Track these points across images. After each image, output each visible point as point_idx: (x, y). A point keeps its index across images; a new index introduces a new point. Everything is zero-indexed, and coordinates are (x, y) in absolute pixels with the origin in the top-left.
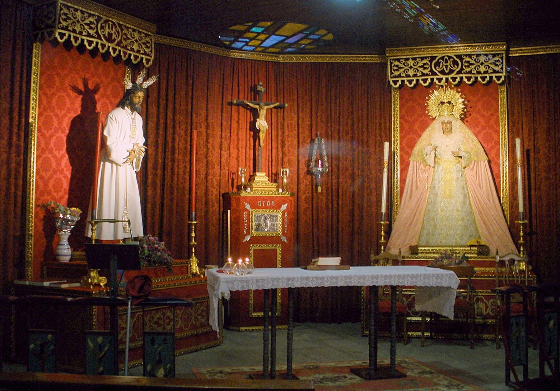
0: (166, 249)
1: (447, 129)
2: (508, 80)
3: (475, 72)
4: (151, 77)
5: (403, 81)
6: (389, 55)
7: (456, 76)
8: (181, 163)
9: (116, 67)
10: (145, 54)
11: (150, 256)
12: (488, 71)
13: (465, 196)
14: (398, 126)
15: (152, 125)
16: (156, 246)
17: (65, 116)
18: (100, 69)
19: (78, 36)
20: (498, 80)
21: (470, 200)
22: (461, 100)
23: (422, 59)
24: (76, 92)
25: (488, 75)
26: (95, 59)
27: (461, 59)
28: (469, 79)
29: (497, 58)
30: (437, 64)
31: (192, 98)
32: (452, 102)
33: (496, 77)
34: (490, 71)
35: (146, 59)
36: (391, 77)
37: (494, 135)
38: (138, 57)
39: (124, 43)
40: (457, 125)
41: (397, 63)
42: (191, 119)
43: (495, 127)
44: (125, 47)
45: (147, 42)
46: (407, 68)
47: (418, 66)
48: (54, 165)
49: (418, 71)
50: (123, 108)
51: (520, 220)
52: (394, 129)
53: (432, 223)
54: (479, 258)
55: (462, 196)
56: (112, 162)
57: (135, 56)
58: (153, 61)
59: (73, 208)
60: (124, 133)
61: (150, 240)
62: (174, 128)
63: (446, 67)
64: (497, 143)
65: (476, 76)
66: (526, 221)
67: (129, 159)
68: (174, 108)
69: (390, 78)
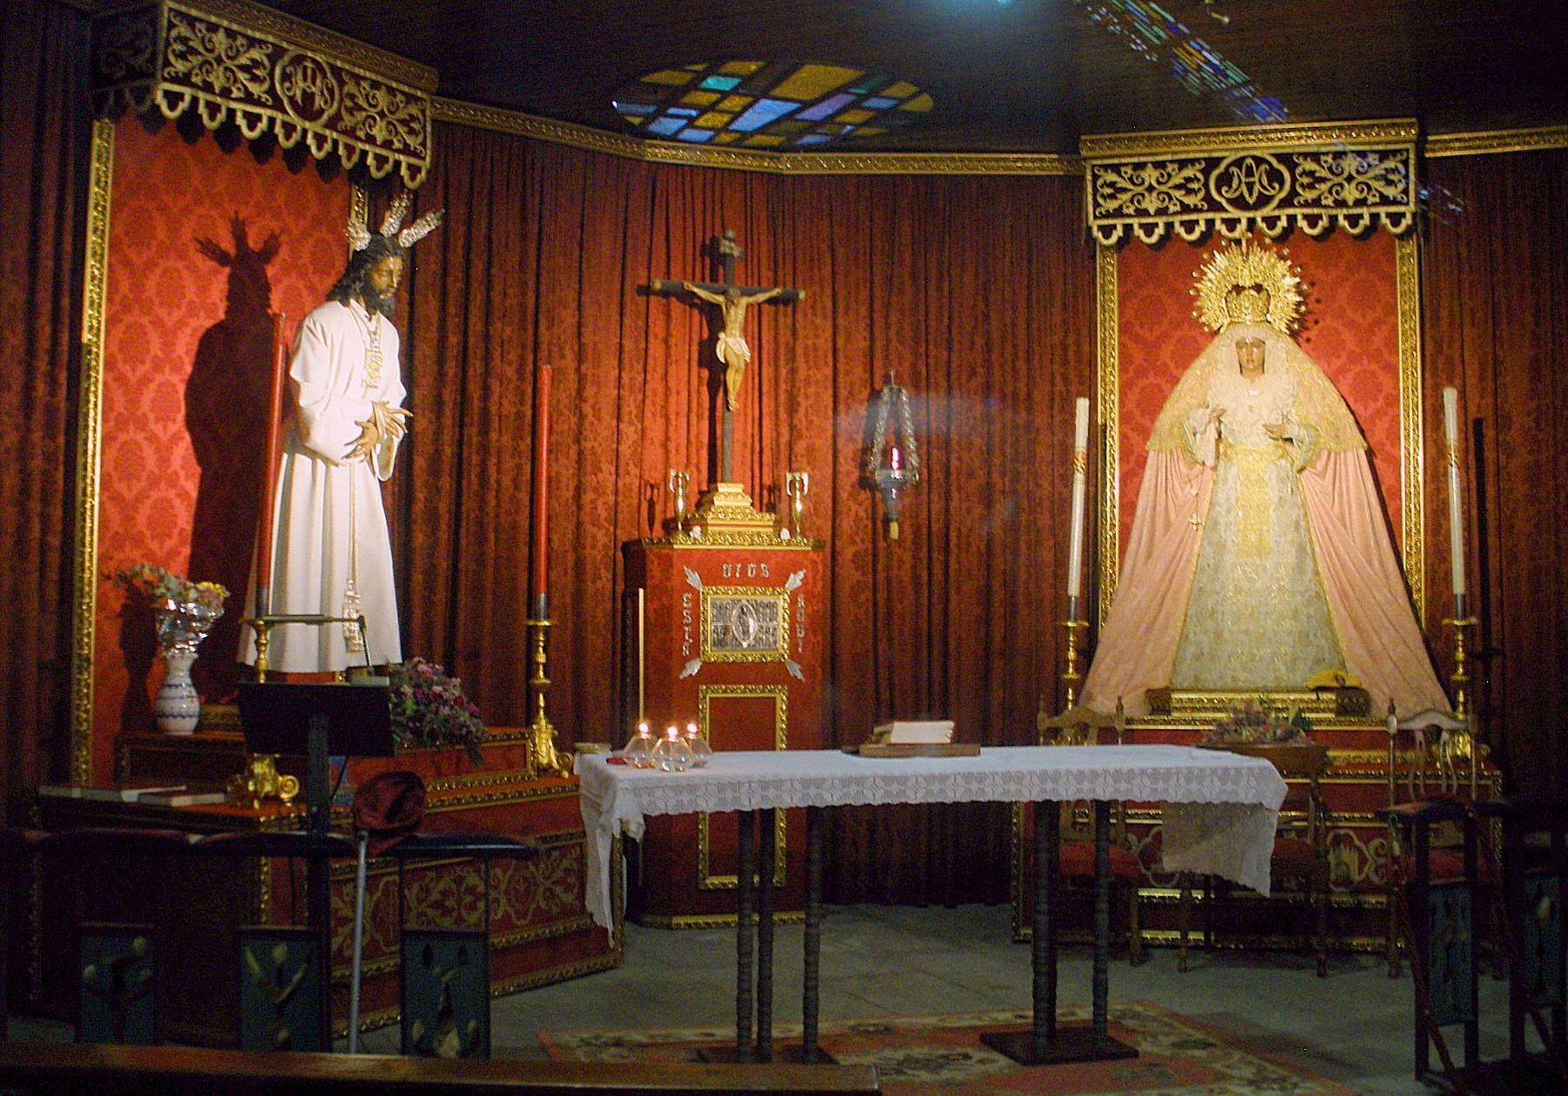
0: (465, 699)
1: (1252, 363)
2: (1424, 225)
3: (1330, 202)
4: (423, 216)
5: (1128, 228)
6: (1090, 154)
7: (1276, 213)
8: (506, 457)
9: (326, 187)
10: (406, 150)
11: (419, 717)
12: (1365, 199)
13: (1302, 550)
14: (1116, 354)
15: (425, 349)
16: (438, 689)
17: (181, 324)
18: (281, 195)
19: (219, 100)
20: (1396, 224)
21: (1315, 561)
22: (1290, 281)
23: (1183, 164)
24: (212, 259)
25: (1365, 211)
26: (267, 167)
27: (1292, 167)
28: (1313, 220)
29: (1390, 164)
30: (1225, 180)
31: (538, 275)
32: (1265, 285)
33: (1388, 215)
34: (1371, 200)
35: (410, 166)
36: (1095, 217)
37: (1384, 378)
38: (386, 159)
39: (348, 120)
40: (1281, 349)
41: (1111, 177)
42: (536, 334)
43: (1386, 356)
44: (351, 133)
45: (413, 118)
46: (1140, 189)
47: (1170, 184)
48: (151, 461)
49: (1170, 198)
50: (345, 303)
51: (1456, 617)
52: (1103, 361)
53: (1210, 625)
54: (1341, 723)
55: (1293, 551)
56: (313, 454)
57: (377, 157)
58: (429, 172)
59: (205, 584)
60: (349, 371)
61: (419, 674)
62: (487, 358)
63: (1250, 186)
64: (1393, 400)
65: (1334, 212)
66: (1474, 620)
67: (360, 447)
68: (488, 302)
69: (1091, 217)
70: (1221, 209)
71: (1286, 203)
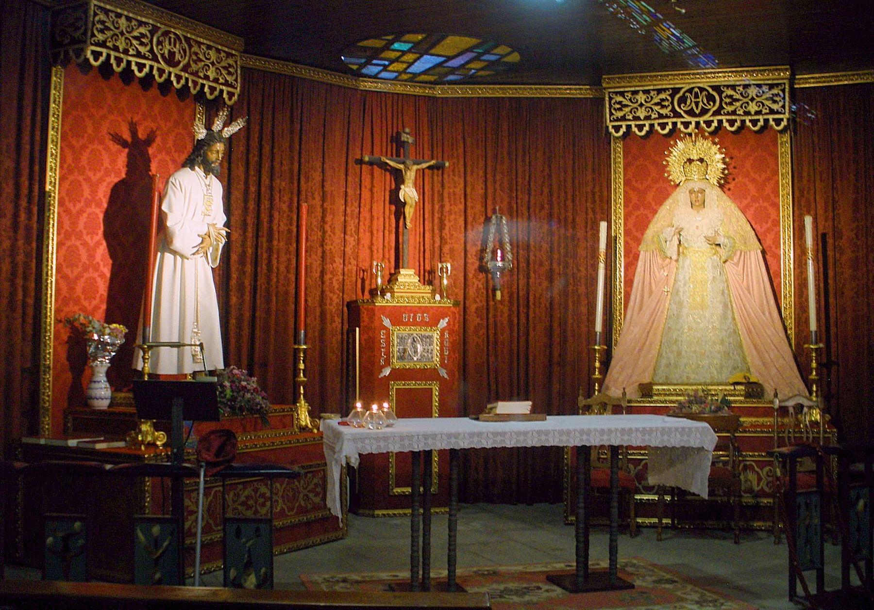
0: (259, 389)
1: (698, 202)
2: (793, 125)
3: (741, 112)
4: (236, 120)
5: (629, 127)
6: (608, 86)
7: (711, 118)
8: (282, 254)
9: (181, 104)
10: (226, 84)
11: (233, 399)
12: (761, 111)
13: (725, 306)
14: (622, 197)
15: (237, 194)
16: (244, 383)
17: (101, 180)
18: (157, 108)
19: (122, 56)
20: (778, 124)
21: (733, 312)
22: (719, 156)
23: (659, 91)
24: (118, 144)
25: (761, 118)
26: (149, 93)
27: (720, 93)
28: (732, 123)
29: (775, 91)
30: (683, 100)
31: (300, 153)
32: (705, 159)
33: (774, 120)
34: (764, 111)
35: (228, 93)
36: (611, 121)
37: (771, 211)
38: (215, 89)
39: (194, 67)
40: (714, 194)
41: (619, 98)
42: (299, 186)
43: (773, 198)
44: (195, 74)
45: (230, 66)
46: (635, 105)
47: (652, 102)
48: (84, 257)
49: (652, 110)
50: (193, 169)
51: (812, 343)
52: (615, 201)
53: (675, 348)
54: (747, 402)
55: (721, 306)
56: (175, 253)
57: (210, 87)
58: (239, 96)
59: (114, 325)
60: (194, 207)
61: (234, 375)
62: (271, 199)
63: (697, 104)
64: (776, 223)
65: (744, 118)
66: (821, 345)
67: (201, 249)
68: (272, 168)
69: (608, 121)
70: (681, 116)
71: (717, 113)
